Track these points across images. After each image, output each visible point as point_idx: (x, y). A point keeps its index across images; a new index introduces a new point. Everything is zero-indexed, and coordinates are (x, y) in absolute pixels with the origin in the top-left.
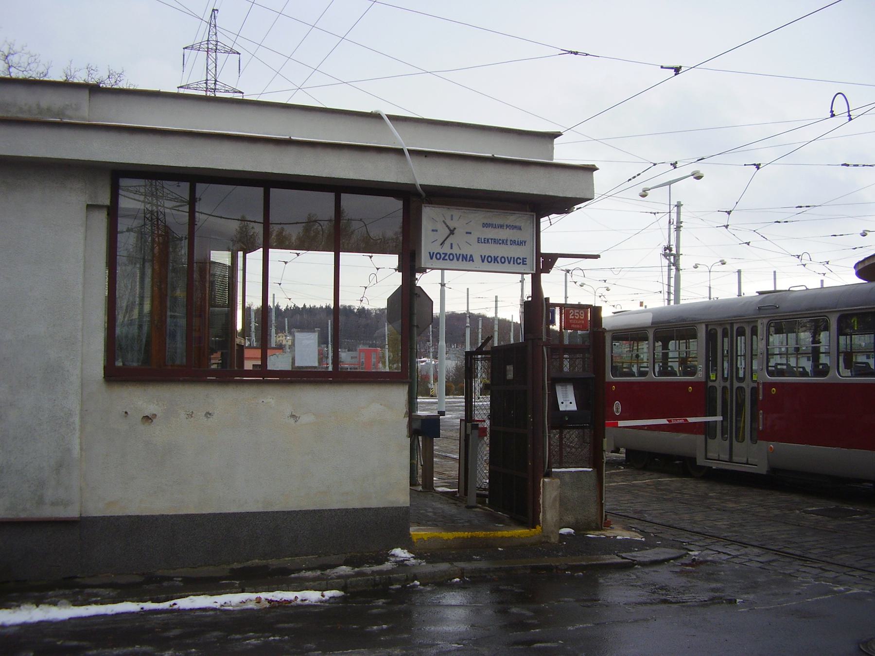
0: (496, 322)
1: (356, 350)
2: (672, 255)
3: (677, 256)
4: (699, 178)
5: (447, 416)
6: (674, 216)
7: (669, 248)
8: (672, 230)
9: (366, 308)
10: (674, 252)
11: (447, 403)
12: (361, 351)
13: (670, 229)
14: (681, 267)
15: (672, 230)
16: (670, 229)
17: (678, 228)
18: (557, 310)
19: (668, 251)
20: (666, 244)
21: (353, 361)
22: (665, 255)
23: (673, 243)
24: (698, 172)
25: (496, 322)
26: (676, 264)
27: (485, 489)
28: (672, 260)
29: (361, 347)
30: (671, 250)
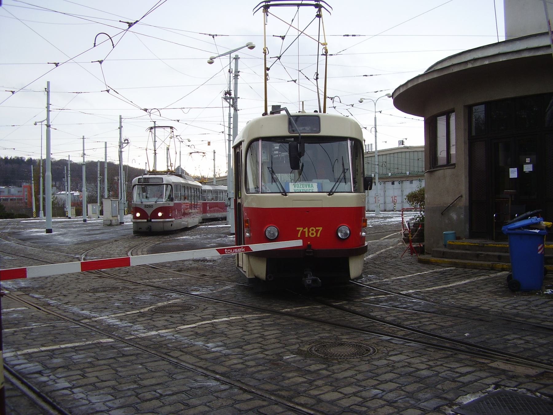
0: (106, 166)
1: (21, 187)
2: (230, 98)
3: (235, 99)
4: (252, 48)
5: (53, 233)
6: (233, 67)
7: (228, 93)
8: (232, 78)
9: (33, 159)
10: (233, 96)
11: (53, 222)
12: (25, 187)
13: (230, 77)
14: (239, 108)
15: (232, 78)
16: (230, 77)
17: (236, 76)
18: (299, 236)
19: (228, 96)
20: (227, 89)
21: (21, 194)
22: (226, 99)
23: (232, 88)
24: (251, 43)
25: (106, 166)
26: (234, 106)
27: (222, 180)
28: (231, 103)
29: (24, 184)
30: (230, 95)
